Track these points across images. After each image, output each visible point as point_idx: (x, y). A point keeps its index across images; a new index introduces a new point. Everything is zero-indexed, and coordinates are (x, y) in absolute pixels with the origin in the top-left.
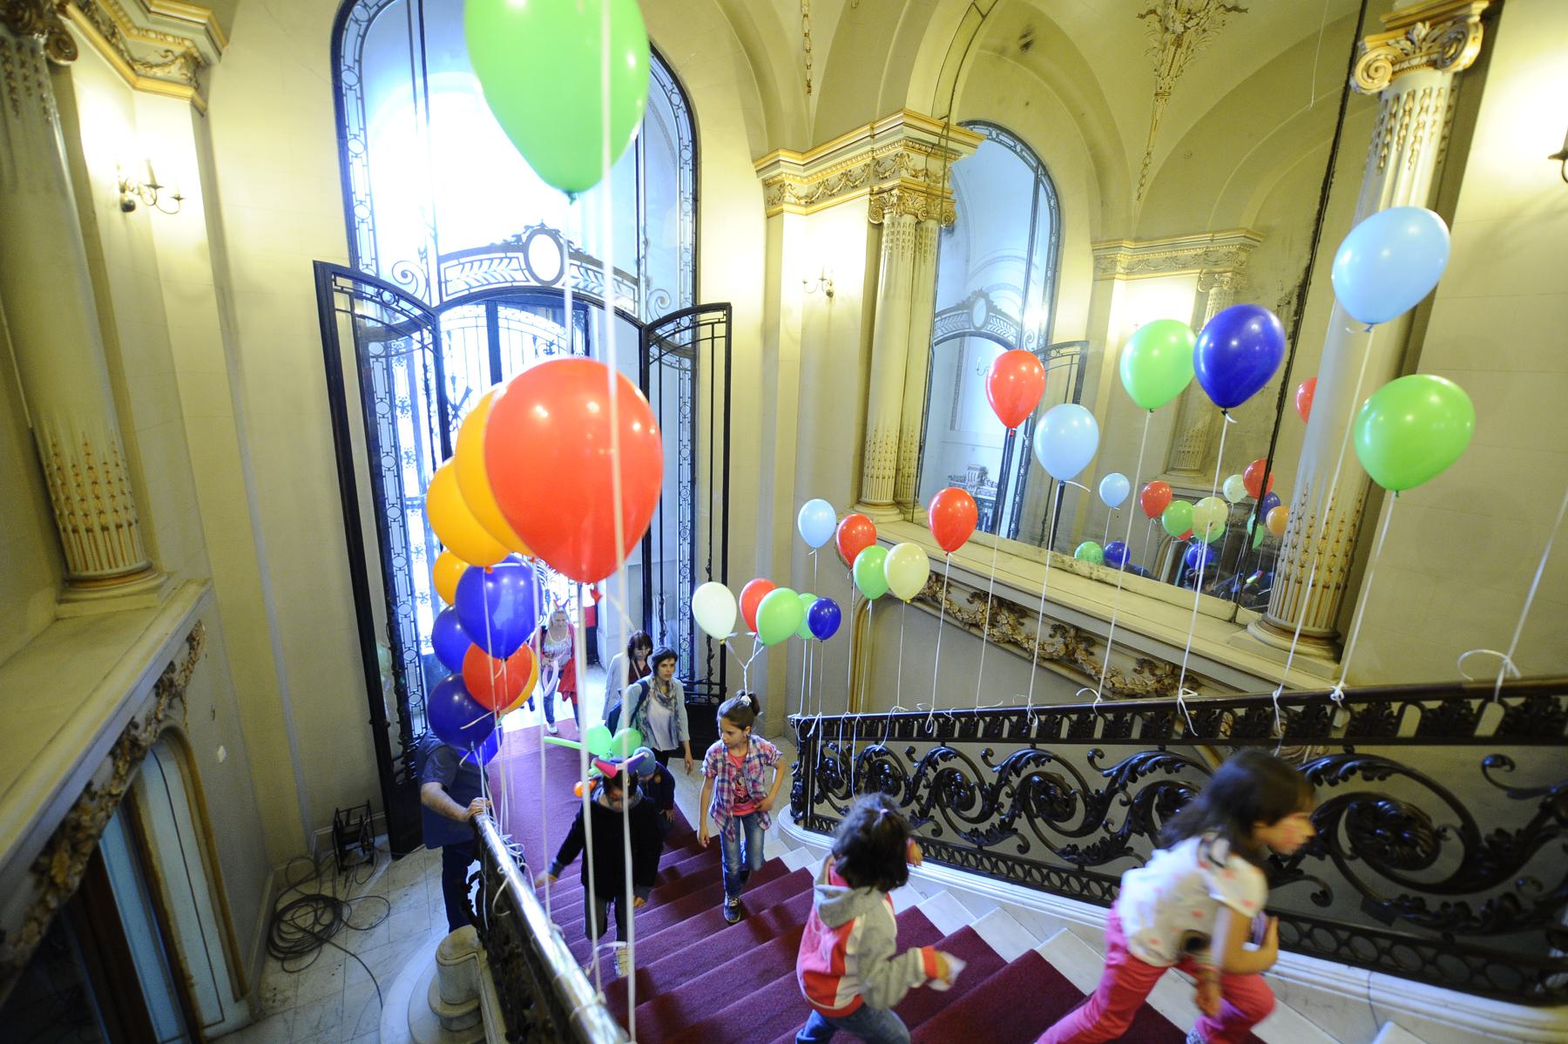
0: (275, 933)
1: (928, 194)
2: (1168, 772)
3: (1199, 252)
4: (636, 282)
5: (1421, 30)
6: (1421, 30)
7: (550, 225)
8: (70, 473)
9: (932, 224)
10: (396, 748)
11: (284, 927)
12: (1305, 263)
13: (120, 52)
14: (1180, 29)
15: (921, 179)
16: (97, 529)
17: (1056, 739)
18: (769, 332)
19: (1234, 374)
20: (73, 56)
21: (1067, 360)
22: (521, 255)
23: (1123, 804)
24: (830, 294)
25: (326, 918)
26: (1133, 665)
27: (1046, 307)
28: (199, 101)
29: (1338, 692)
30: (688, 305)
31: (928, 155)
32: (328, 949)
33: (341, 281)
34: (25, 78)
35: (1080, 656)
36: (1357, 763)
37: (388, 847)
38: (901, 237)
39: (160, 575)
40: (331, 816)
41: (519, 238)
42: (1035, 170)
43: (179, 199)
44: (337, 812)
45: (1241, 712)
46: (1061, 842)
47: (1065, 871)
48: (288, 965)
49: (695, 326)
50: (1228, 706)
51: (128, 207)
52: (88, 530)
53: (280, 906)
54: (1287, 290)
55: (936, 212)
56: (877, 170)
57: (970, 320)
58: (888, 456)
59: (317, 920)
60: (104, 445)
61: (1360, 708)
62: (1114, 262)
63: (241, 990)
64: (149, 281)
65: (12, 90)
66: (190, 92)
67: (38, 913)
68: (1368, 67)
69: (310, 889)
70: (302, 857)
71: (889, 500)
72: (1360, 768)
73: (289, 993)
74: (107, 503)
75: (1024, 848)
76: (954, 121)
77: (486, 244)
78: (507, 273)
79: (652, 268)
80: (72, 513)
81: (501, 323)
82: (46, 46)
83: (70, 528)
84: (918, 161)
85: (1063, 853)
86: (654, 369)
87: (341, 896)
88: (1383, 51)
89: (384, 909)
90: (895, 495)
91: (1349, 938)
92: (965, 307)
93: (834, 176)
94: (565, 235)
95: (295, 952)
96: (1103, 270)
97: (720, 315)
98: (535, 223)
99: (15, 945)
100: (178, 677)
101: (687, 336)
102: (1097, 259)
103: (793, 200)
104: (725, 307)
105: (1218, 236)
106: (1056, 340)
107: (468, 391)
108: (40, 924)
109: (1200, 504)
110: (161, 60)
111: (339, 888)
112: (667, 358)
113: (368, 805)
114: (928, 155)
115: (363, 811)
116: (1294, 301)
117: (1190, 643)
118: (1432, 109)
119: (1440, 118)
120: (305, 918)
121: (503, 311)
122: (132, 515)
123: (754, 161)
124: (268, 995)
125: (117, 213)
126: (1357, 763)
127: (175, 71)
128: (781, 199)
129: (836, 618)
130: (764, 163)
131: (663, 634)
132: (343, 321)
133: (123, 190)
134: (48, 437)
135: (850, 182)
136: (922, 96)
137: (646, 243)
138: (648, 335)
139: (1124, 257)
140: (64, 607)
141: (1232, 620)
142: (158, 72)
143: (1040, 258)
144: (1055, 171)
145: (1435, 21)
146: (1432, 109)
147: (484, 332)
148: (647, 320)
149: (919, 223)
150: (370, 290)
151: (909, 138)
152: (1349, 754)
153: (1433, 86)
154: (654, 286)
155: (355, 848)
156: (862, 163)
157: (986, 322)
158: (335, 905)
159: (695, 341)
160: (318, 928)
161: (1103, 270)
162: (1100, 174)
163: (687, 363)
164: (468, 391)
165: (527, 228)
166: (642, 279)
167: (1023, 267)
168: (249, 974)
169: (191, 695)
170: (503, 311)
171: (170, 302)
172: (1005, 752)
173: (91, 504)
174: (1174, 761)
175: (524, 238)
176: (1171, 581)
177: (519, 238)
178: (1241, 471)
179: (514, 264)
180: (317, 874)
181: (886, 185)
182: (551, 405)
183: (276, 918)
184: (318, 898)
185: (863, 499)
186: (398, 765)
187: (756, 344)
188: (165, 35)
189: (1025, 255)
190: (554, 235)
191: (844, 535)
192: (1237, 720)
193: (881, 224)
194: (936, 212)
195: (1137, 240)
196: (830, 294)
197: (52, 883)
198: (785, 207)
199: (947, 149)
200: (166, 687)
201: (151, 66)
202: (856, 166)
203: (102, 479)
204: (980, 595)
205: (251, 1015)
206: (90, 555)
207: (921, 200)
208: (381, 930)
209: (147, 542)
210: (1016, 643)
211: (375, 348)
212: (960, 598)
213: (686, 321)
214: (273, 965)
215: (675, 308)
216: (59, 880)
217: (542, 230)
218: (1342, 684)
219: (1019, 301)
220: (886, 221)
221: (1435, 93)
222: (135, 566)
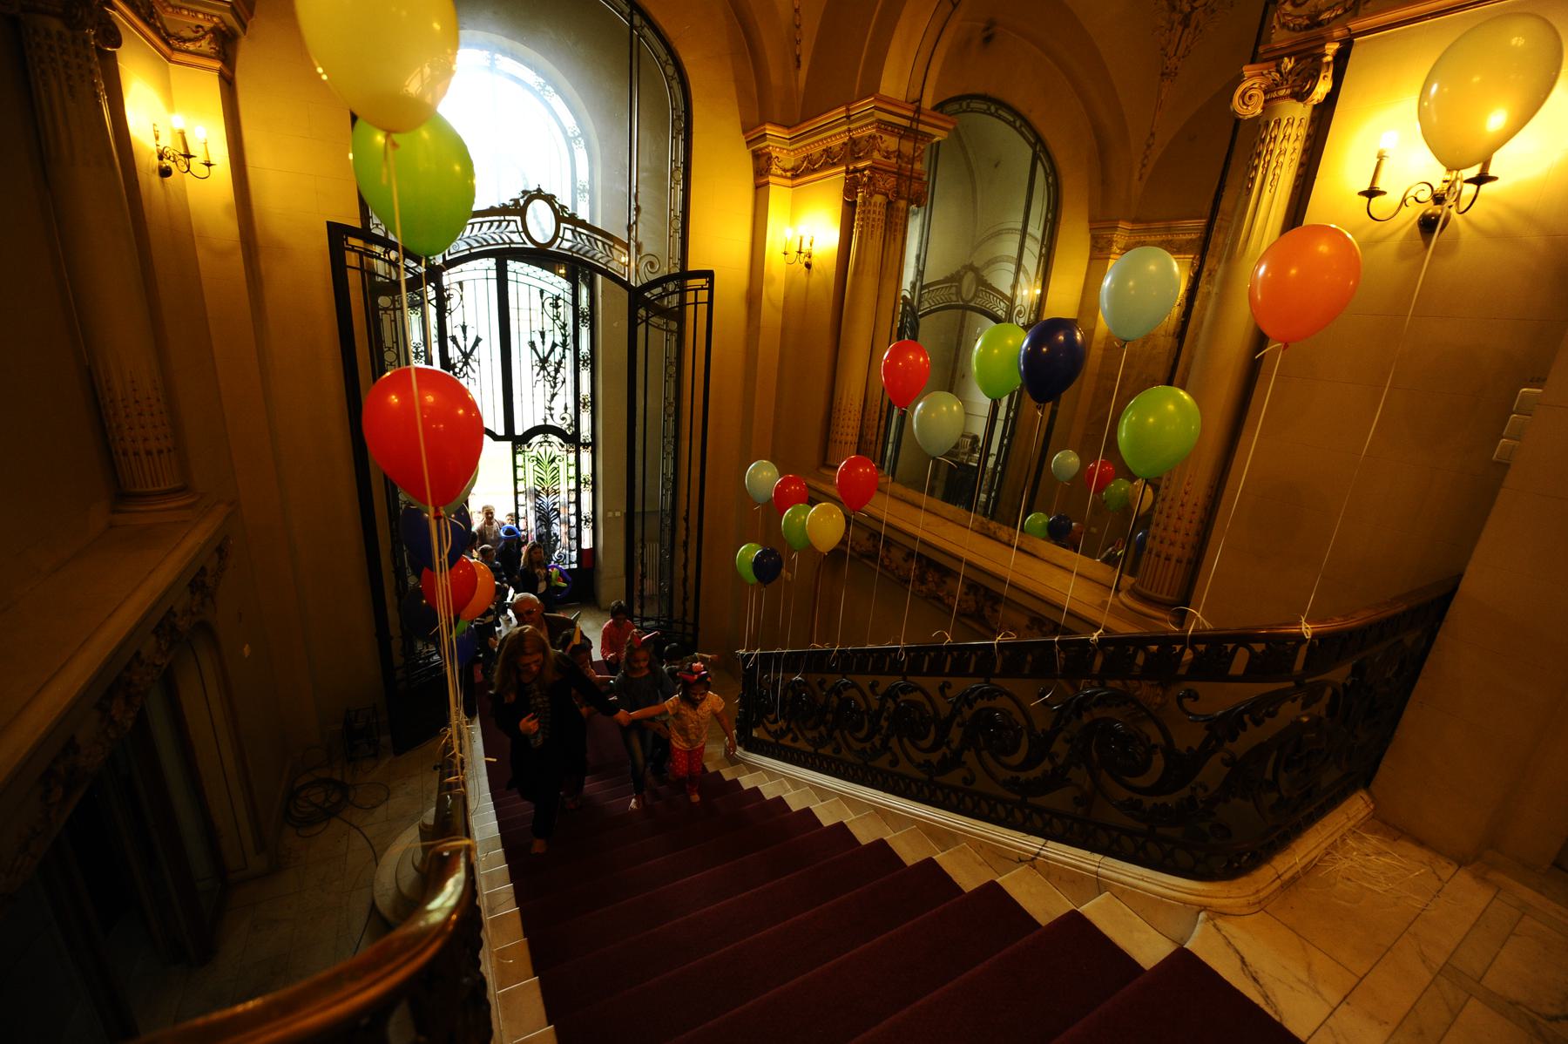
1: (899, 174)
4: (628, 247)
5: (1288, 64)
6: (1288, 64)
7: (547, 190)
10: (398, 660)
13: (156, 31)
14: (1187, 8)
16: (1163, 556)
17: (920, 674)
18: (753, 296)
20: (118, 44)
22: (518, 219)
23: (959, 725)
28: (226, 71)
33: (353, 241)
34: (79, 66)
35: (987, 612)
38: (872, 216)
41: (516, 201)
42: (1033, 146)
46: (920, 757)
49: (683, 291)
51: (165, 172)
52: (135, 454)
56: (853, 150)
58: (852, 423)
62: (1110, 243)
64: (183, 232)
65: (69, 77)
66: (218, 65)
68: (1244, 93)
75: (895, 762)
76: (928, 103)
79: (643, 233)
81: (510, 276)
82: (95, 36)
84: (891, 142)
85: (919, 766)
86: (641, 329)
88: (1257, 80)
93: (817, 150)
96: (1099, 251)
97: (702, 282)
98: (532, 188)
101: (674, 300)
104: (709, 275)
107: (478, 340)
110: (192, 35)
118: (1293, 137)
119: (1299, 146)
121: (512, 265)
123: (744, 132)
125: (156, 178)
127: (204, 45)
129: (778, 566)
132: (354, 278)
133: (161, 157)
135: (829, 160)
136: (893, 83)
137: (638, 209)
139: (1120, 238)
142: (191, 46)
143: (1036, 229)
145: (1299, 56)
146: (1293, 137)
147: (493, 284)
149: (889, 203)
150: (378, 249)
151: (880, 121)
153: (1296, 115)
154: (645, 250)
157: (976, 295)
159: (683, 303)
161: (1099, 251)
163: (674, 326)
164: (478, 340)
165: (525, 192)
166: (633, 243)
167: (1018, 237)
170: (512, 265)
171: (201, 254)
172: (886, 682)
179: (512, 227)
181: (861, 165)
182: (399, 395)
187: (741, 311)
188: (197, 12)
189: (1020, 226)
195: (1133, 222)
198: (771, 179)
199: (917, 132)
201: (185, 41)
202: (836, 143)
204: (910, 554)
210: (939, 599)
211: (384, 301)
212: (897, 555)
215: (665, 271)
217: (539, 194)
221: (1296, 123)
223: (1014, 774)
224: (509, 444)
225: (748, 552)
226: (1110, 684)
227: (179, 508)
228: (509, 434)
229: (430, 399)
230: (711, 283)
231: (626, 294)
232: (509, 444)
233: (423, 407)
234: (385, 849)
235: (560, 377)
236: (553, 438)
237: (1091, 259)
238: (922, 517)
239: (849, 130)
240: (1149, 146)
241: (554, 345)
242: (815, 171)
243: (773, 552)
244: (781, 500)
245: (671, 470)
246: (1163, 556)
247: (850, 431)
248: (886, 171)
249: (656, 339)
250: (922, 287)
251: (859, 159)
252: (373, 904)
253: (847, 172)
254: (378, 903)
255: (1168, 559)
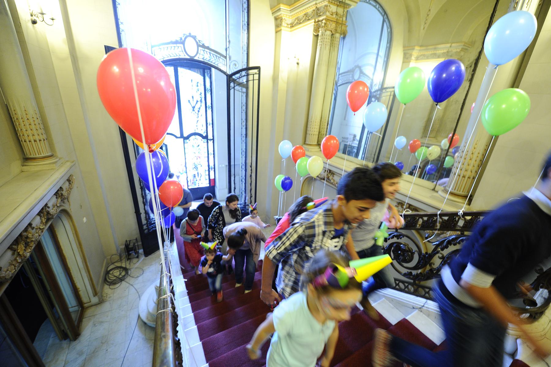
0: (107, 277)
1: (337, 22)
2: (398, 239)
3: (445, 51)
4: (226, 57)
8: (21, 121)
9: (337, 35)
10: (144, 222)
11: (110, 276)
12: (479, 50)
15: (334, 16)
18: (275, 79)
19: (442, 90)
21: (389, 94)
24: (298, 64)
25: (123, 273)
26: (395, 204)
27: (383, 73)
29: (461, 212)
30: (245, 67)
31: (338, 6)
32: (123, 282)
35: (330, 178)
36: (464, 238)
37: (143, 253)
38: (325, 40)
39: (56, 158)
40: (124, 243)
43: (53, 19)
44: (126, 241)
45: (425, 219)
47: (407, 282)
48: (111, 287)
49: (248, 75)
50: (421, 216)
51: (34, 22)
52: (30, 141)
53: (109, 269)
54: (471, 61)
55: (339, 30)
56: (318, 12)
57: (353, 77)
59: (120, 274)
60: (32, 111)
61: (468, 218)
62: (411, 55)
63: (95, 294)
64: (46, 53)
67: (14, 263)
69: (118, 264)
70: (115, 255)
71: (316, 143)
72: (465, 239)
73: (111, 295)
74: (35, 132)
77: (169, 41)
78: (178, 53)
79: (231, 52)
80: (23, 135)
83: (23, 140)
86: (232, 91)
87: (128, 267)
89: (142, 272)
90: (318, 142)
91: (429, 291)
92: (351, 71)
93: (301, 15)
94: (198, 38)
95: (113, 283)
99: (6, 272)
100: (64, 193)
101: (244, 80)
102: (405, 54)
103: (286, 25)
104: (258, 68)
105: (453, 45)
106: (385, 86)
108: (15, 266)
109: (430, 148)
111: (128, 264)
112: (237, 88)
113: (136, 239)
114: (338, 6)
115: (135, 241)
116: (473, 66)
117: (409, 194)
120: (117, 273)
121: (180, 70)
122: (44, 137)
123: (271, 9)
124: (105, 295)
125: (30, 24)
126: (464, 238)
128: (281, 25)
129: (291, 184)
130: (275, 9)
131: (235, 188)
133: (32, 16)
134: (12, 107)
135: (307, 17)
137: (229, 42)
138: (230, 78)
139: (415, 53)
140: (25, 167)
141: (434, 190)
143: (382, 53)
144: (388, 12)
148: (229, 73)
149: (332, 35)
152: (462, 235)
154: (232, 59)
155: (133, 253)
156: (312, 9)
157: (359, 78)
158: (126, 269)
159: (248, 81)
160: (121, 276)
161: (407, 58)
162: (409, 19)
163: (244, 90)
165: (184, 35)
166: (228, 56)
167: (375, 56)
168: (98, 289)
169: (71, 199)
170: (180, 70)
173: (29, 132)
174: (400, 235)
175: (183, 39)
176: (420, 177)
177: (181, 39)
178: (447, 137)
180: (121, 260)
181: (321, 18)
183: (107, 273)
184: (121, 267)
185: (307, 142)
186: (145, 227)
189: (376, 52)
190: (194, 38)
191: (293, 153)
192: (424, 222)
193: (318, 35)
194: (339, 30)
195: (421, 46)
196: (298, 64)
197: (19, 254)
198: (282, 28)
200: (58, 194)
202: (310, 11)
203: (32, 123)
205: (99, 301)
206: (32, 150)
207: (334, 25)
208: (140, 278)
209: (51, 146)
213: (244, 73)
214: (106, 287)
216: (21, 253)
218: (463, 209)
219: (373, 69)
220: (320, 34)
222: (47, 155)
223: (409, 271)
224: (182, 139)
225: (279, 179)
226: (466, 233)
227: (50, 164)
228: (182, 136)
229: (141, 70)
230: (259, 71)
231: (226, 77)
232: (182, 139)
233: (137, 75)
234: (143, 293)
235: (200, 115)
236: (197, 137)
237: (403, 62)
238: (345, 162)
239: (316, 4)
240: (428, 15)
241: (197, 101)
242: (300, 23)
243: (288, 178)
244: (295, 157)
245: (244, 147)
246: (461, 176)
247: (316, 130)
248: (332, 21)
249: (238, 95)
250: (339, 75)
251: (320, 16)
252: (139, 316)
253: (315, 22)
254: (141, 315)
255: (464, 177)
